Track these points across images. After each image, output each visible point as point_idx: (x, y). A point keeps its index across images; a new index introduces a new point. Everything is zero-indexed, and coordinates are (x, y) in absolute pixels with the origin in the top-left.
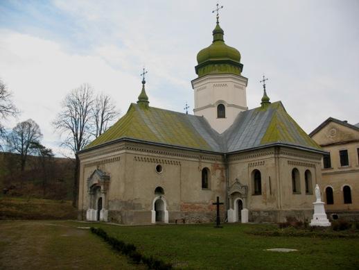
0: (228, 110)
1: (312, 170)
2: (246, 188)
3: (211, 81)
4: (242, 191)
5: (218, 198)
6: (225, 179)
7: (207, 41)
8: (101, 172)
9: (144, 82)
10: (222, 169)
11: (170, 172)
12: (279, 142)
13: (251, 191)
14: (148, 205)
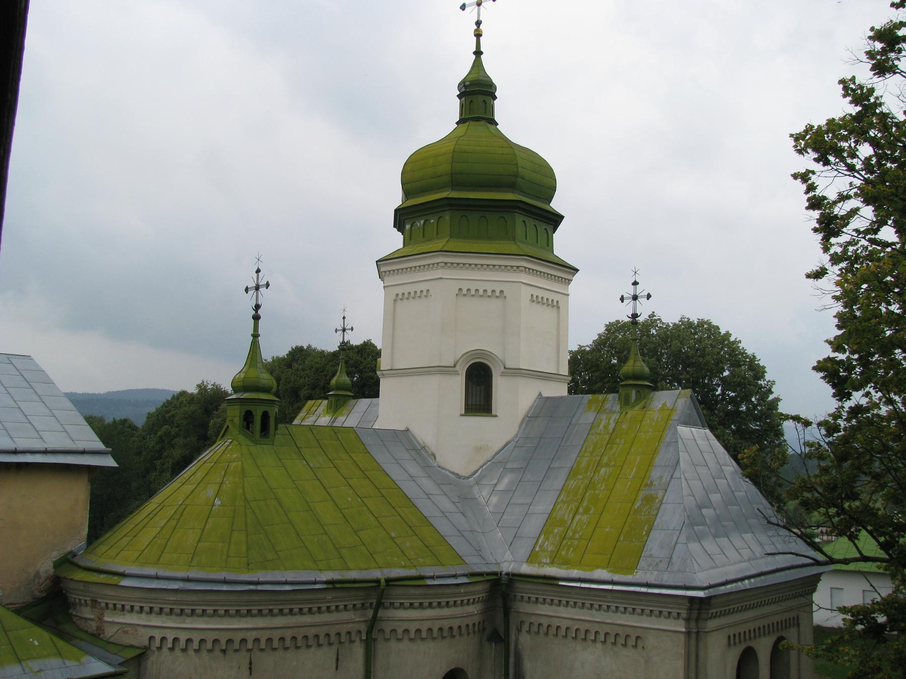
0: (500, 386)
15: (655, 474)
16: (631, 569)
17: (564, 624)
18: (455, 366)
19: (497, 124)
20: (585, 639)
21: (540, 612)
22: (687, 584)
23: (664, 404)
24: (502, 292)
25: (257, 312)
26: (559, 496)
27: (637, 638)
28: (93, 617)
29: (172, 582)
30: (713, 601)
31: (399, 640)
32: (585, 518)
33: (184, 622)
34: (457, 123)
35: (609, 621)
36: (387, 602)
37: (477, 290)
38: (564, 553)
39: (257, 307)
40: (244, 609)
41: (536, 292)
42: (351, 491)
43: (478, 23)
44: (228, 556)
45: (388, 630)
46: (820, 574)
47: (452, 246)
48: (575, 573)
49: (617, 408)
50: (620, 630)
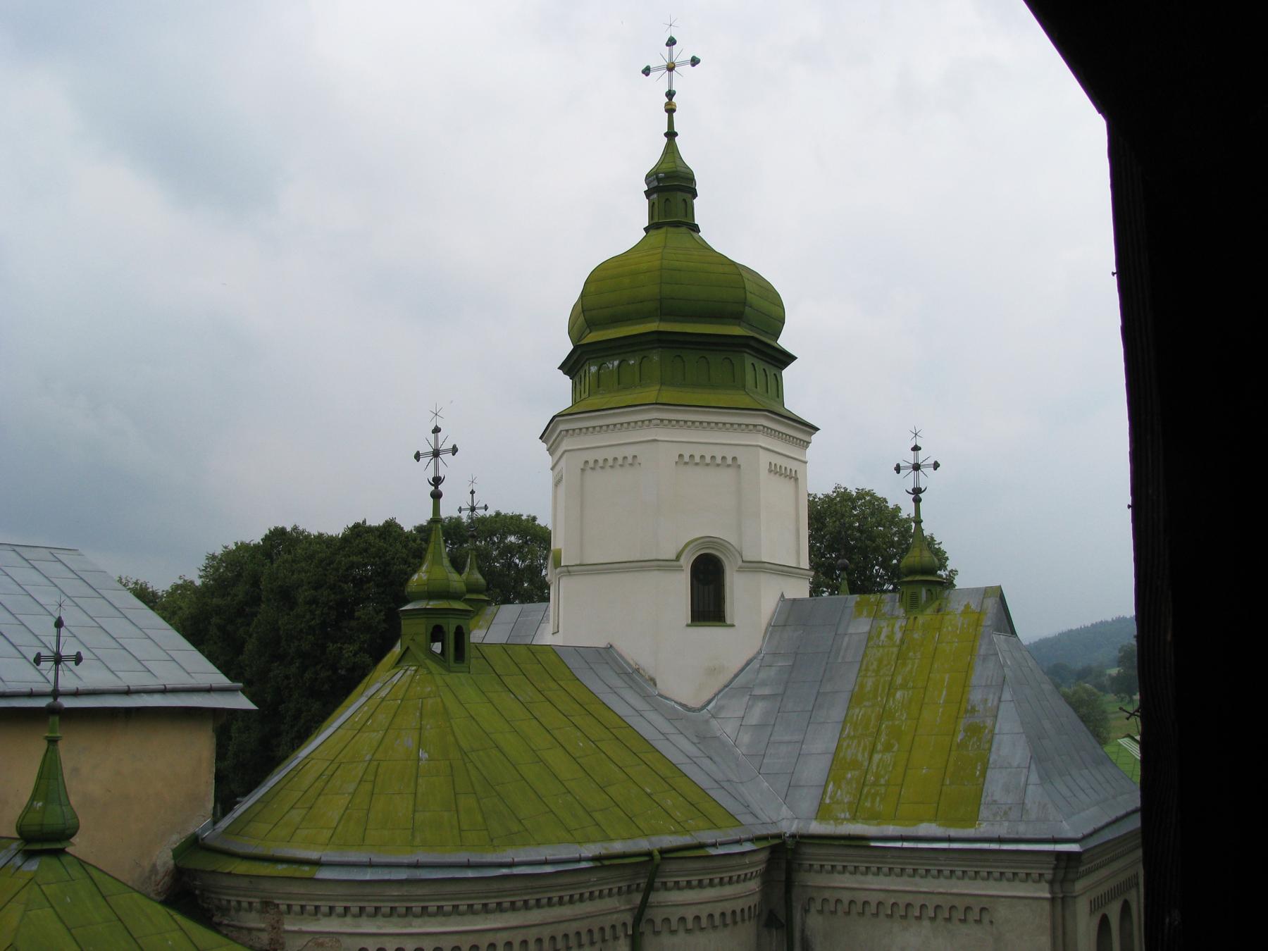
0: (737, 587)
3: (662, 434)
15: (976, 696)
16: (972, 820)
17: (874, 898)
18: (678, 558)
20: (905, 917)
21: (836, 884)
22: (1056, 836)
23: (967, 606)
24: (734, 459)
25: (436, 487)
26: (843, 730)
27: (982, 909)
28: (263, 926)
29: (394, 870)
30: (1084, 857)
31: (673, 932)
32: (888, 757)
33: (411, 925)
34: (646, 229)
35: (941, 890)
36: (657, 884)
37: (702, 457)
38: (868, 804)
39: (437, 481)
40: (492, 903)
41: (590, 456)
42: (579, 734)
43: (670, 94)
44: (460, 830)
45: (658, 921)
46: (215, 823)
47: (668, 395)
48: (891, 830)
49: (900, 612)
50: (956, 902)
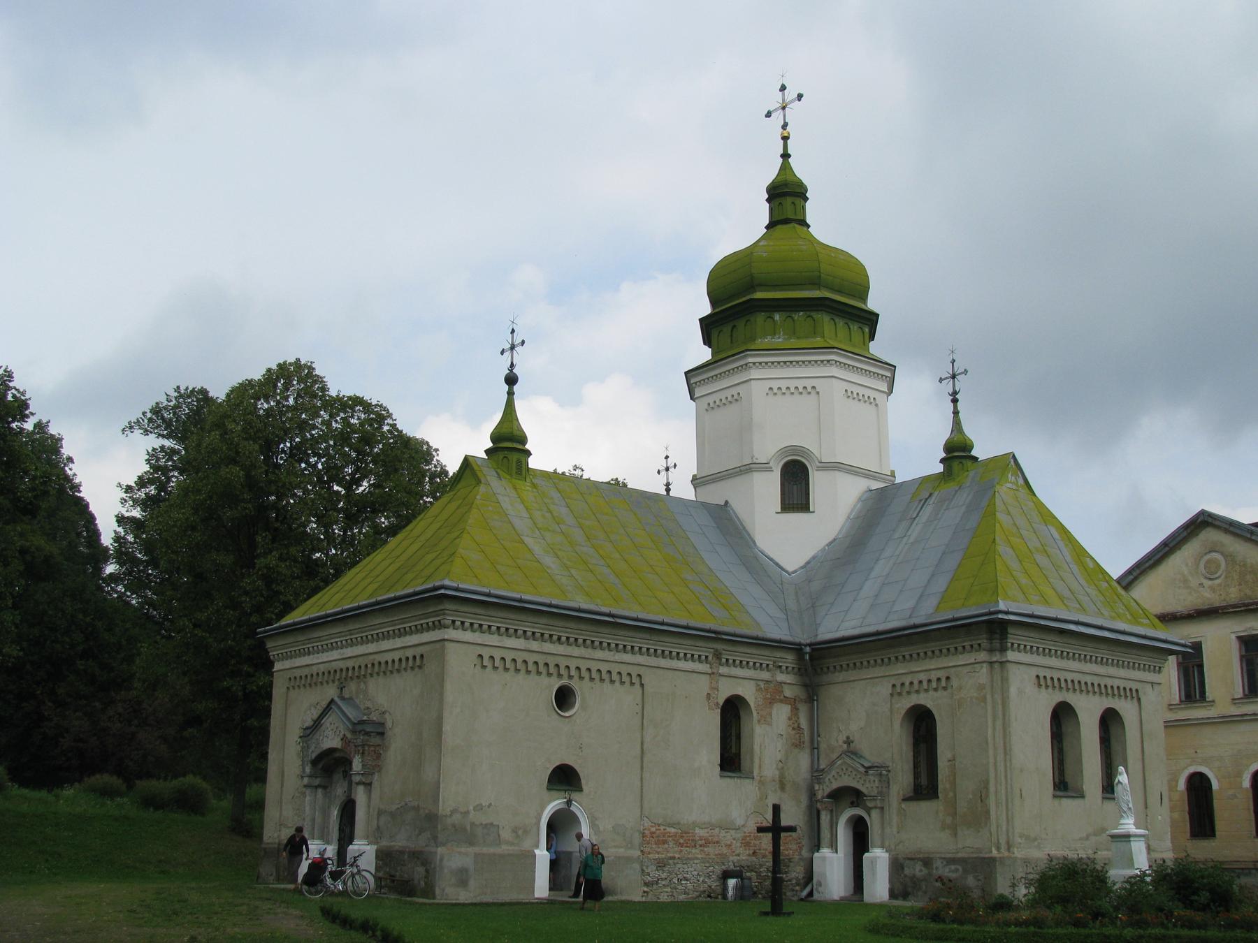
0: (819, 483)
1: (1126, 709)
2: (880, 771)
4: (868, 786)
5: (776, 809)
6: (809, 739)
7: (743, 225)
8: (357, 707)
9: (511, 380)
10: (793, 702)
11: (603, 707)
12: (1002, 606)
13: (902, 779)
14: (521, 831)
19: (808, 226)
34: (767, 227)
41: (851, 388)
